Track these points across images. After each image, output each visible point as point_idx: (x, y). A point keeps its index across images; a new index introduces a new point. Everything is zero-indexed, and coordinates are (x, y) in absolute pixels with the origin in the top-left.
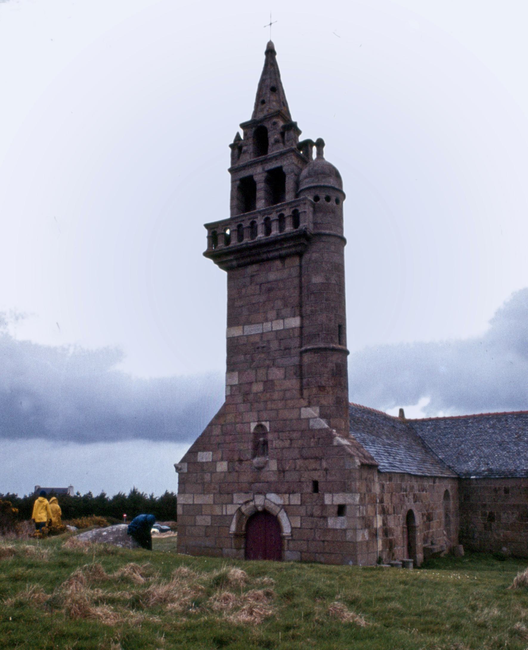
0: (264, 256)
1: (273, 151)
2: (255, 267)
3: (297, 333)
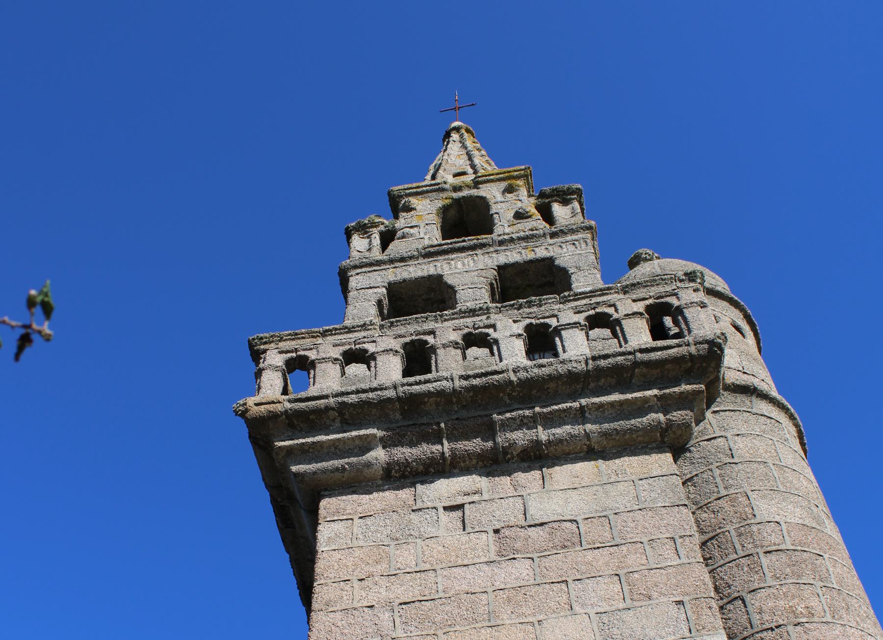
0: (520, 437)
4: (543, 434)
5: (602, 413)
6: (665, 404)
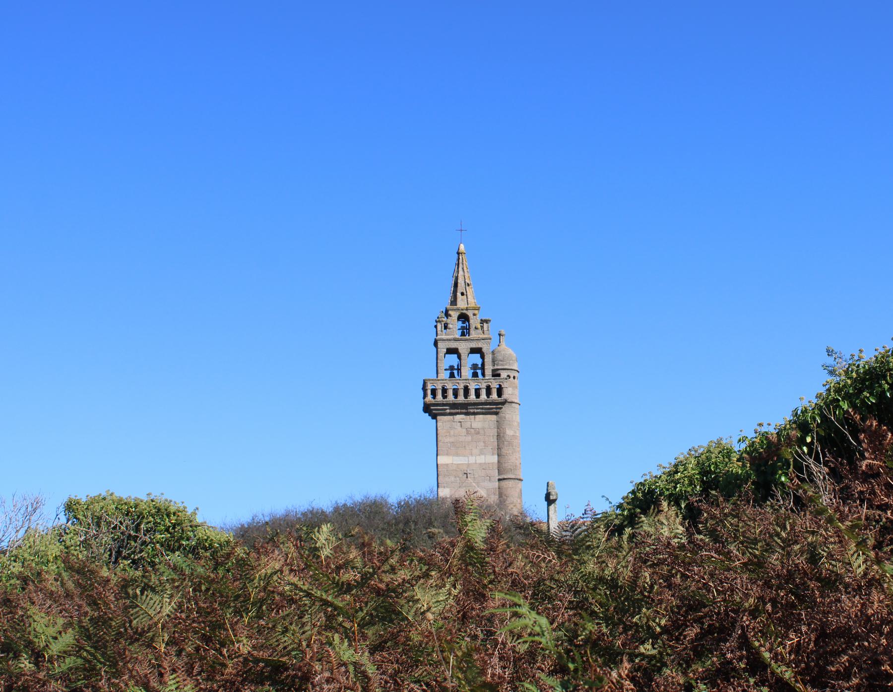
1: (474, 334)
2: (462, 416)
3: (496, 466)
4: (476, 411)
5: (482, 409)
6: (496, 408)
